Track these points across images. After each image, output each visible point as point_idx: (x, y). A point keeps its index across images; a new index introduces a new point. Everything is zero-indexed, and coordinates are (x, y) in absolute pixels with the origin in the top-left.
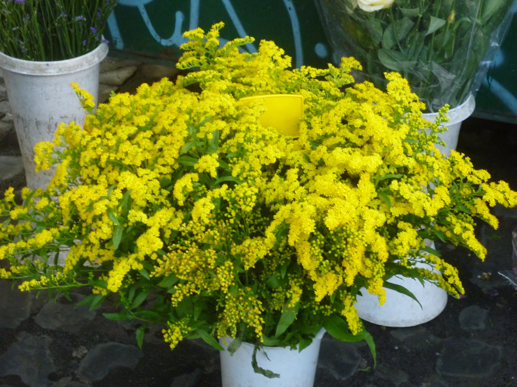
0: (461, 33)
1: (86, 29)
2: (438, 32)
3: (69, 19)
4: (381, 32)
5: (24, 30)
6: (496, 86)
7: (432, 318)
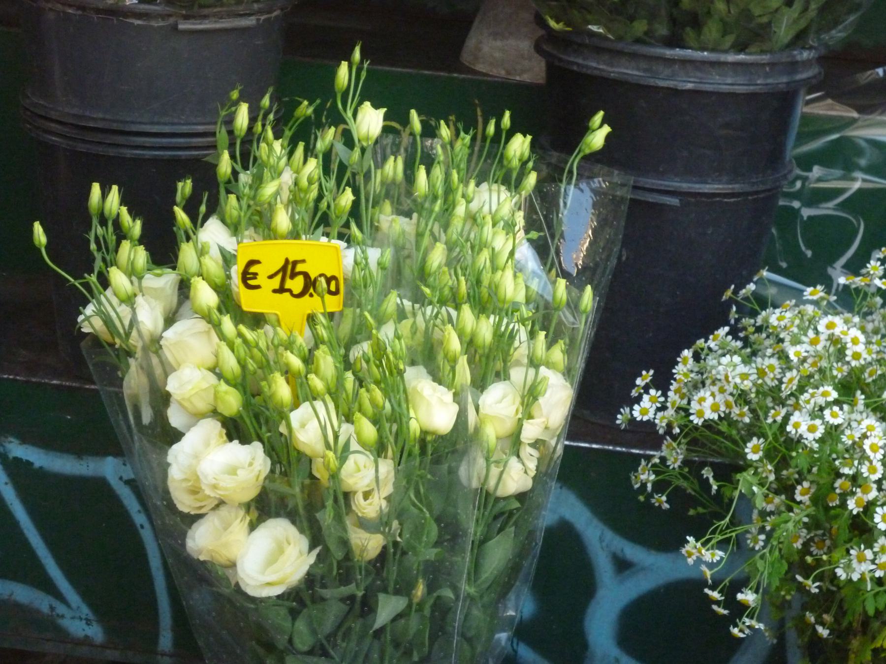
0: (441, 612)
1: (260, 117)
4: (287, 624)
7: (590, 610)
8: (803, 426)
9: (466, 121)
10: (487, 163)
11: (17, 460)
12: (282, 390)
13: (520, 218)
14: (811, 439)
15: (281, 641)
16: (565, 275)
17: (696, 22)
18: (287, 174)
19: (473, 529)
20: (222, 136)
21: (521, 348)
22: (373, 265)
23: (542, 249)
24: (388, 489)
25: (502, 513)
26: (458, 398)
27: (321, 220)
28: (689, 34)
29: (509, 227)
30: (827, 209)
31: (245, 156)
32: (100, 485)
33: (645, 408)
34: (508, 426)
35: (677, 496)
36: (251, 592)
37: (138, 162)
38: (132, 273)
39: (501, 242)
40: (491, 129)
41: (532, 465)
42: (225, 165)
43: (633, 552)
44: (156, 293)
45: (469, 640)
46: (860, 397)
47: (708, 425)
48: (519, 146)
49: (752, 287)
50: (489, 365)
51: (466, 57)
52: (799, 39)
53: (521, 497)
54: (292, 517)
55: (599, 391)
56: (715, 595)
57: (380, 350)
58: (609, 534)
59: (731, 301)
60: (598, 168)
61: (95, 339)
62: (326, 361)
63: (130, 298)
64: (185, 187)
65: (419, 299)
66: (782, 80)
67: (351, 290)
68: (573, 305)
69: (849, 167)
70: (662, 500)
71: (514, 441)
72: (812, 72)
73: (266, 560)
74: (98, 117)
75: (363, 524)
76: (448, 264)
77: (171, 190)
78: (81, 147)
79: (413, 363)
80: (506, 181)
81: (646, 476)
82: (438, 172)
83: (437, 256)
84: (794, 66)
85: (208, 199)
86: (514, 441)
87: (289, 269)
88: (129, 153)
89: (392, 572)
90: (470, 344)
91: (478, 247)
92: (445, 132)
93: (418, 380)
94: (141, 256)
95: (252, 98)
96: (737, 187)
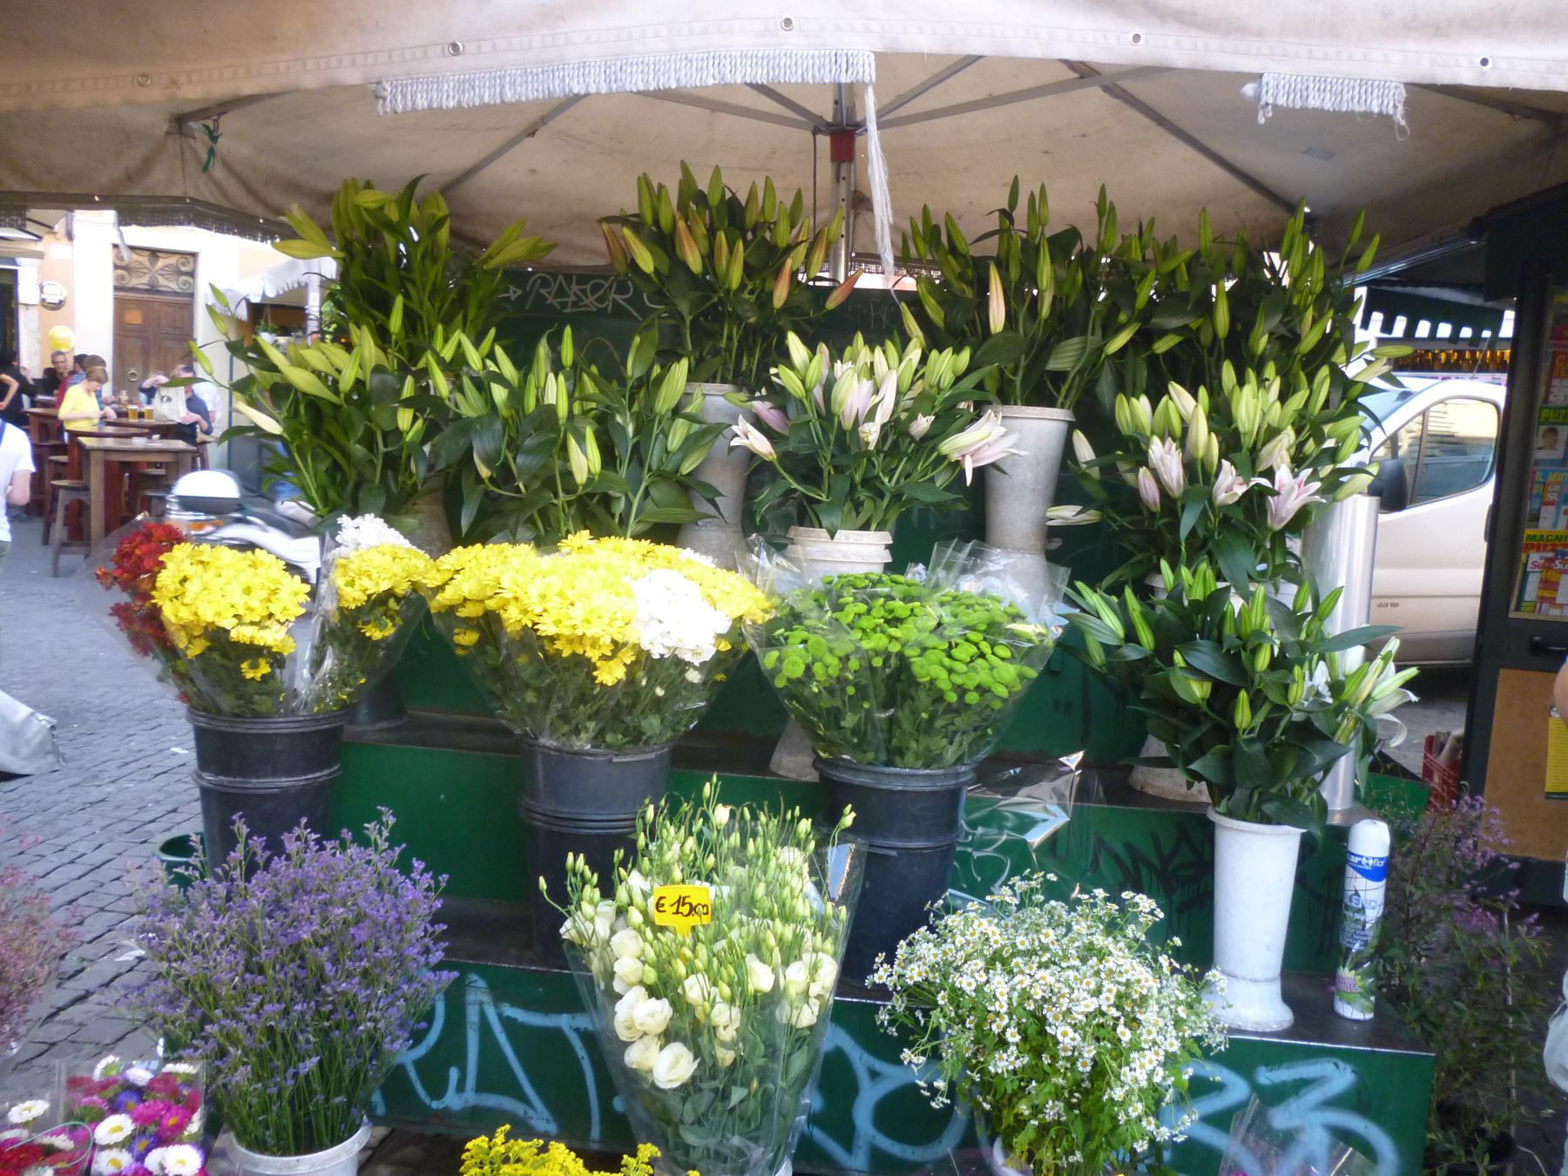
0: (767, 1098)
2: (742, 1102)
3: (327, 1100)
5: (273, 1117)
6: (818, 1135)
8: (966, 983)
9: (774, 811)
10: (787, 836)
11: (508, 1018)
12: (681, 969)
13: (806, 869)
14: (969, 990)
15: (676, 1118)
16: (832, 900)
17: (901, 752)
18: (676, 844)
19: (783, 1045)
20: (639, 824)
21: (808, 942)
22: (725, 897)
23: (819, 885)
24: (737, 1024)
25: (800, 1038)
26: (774, 971)
27: (695, 872)
28: (897, 759)
29: (800, 875)
30: (988, 852)
31: (652, 836)
32: (557, 1033)
33: (882, 975)
34: (802, 987)
35: (902, 1028)
36: (662, 1086)
37: (588, 836)
38: (591, 902)
39: (795, 882)
40: (789, 816)
41: (816, 1009)
42: (642, 840)
43: (880, 1066)
44: (605, 915)
45: (784, 1116)
46: (998, 965)
47: (917, 985)
48: (805, 825)
49: (941, 902)
50: (790, 952)
51: (773, 766)
52: (959, 761)
53: (811, 1028)
54: (684, 1041)
55: (854, 966)
56: (922, 1084)
57: (731, 945)
58: (866, 1056)
59: (929, 911)
60: (850, 837)
61: (572, 944)
62: (702, 950)
63: (590, 918)
64: (619, 854)
65: (752, 915)
66: (951, 783)
67: (714, 912)
68: (836, 917)
69: (1001, 829)
70: (893, 1031)
71: (806, 996)
72: (970, 776)
73: (669, 1067)
74: (565, 811)
75: (723, 1044)
76: (767, 894)
77: (611, 853)
78: (555, 829)
79: (748, 952)
80: (798, 845)
81: (883, 1017)
82: (760, 840)
83: (760, 891)
84: (958, 775)
85: (633, 857)
86: (806, 996)
87: (681, 901)
88: (584, 831)
89: (739, 1075)
90: (780, 940)
91: (783, 885)
92: (763, 818)
93: (752, 961)
94: (597, 892)
95: (655, 802)
96: (929, 844)
